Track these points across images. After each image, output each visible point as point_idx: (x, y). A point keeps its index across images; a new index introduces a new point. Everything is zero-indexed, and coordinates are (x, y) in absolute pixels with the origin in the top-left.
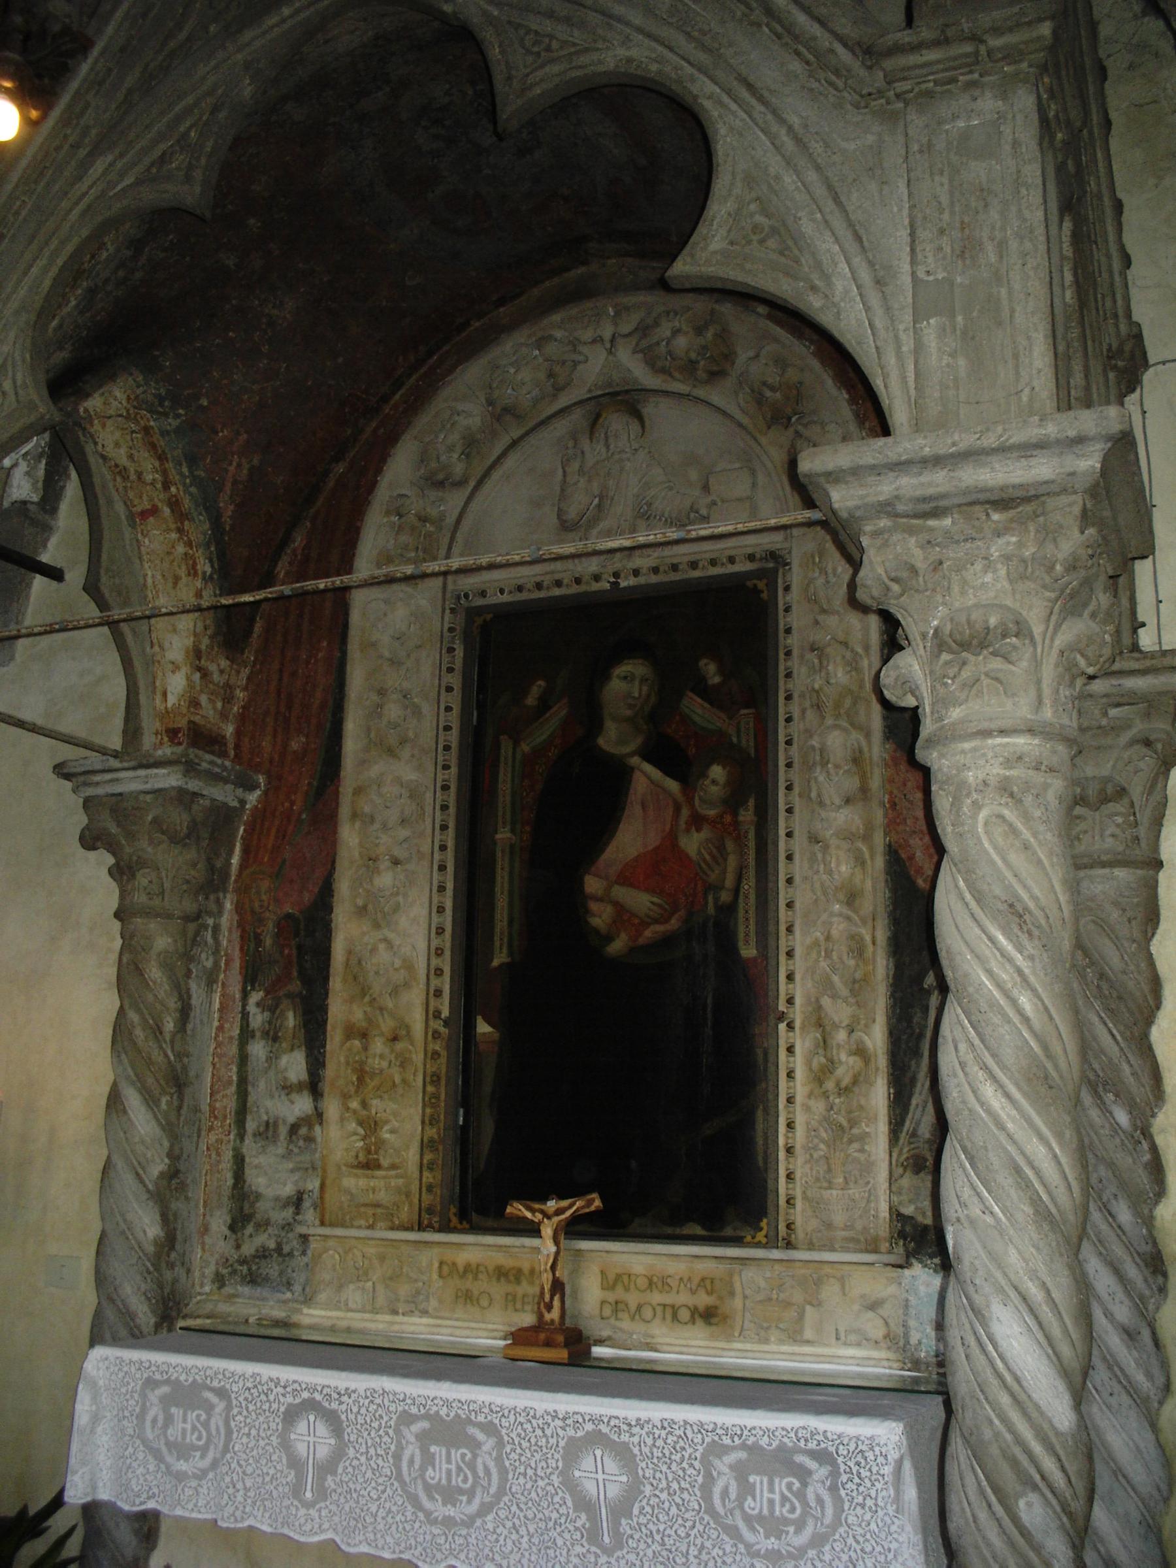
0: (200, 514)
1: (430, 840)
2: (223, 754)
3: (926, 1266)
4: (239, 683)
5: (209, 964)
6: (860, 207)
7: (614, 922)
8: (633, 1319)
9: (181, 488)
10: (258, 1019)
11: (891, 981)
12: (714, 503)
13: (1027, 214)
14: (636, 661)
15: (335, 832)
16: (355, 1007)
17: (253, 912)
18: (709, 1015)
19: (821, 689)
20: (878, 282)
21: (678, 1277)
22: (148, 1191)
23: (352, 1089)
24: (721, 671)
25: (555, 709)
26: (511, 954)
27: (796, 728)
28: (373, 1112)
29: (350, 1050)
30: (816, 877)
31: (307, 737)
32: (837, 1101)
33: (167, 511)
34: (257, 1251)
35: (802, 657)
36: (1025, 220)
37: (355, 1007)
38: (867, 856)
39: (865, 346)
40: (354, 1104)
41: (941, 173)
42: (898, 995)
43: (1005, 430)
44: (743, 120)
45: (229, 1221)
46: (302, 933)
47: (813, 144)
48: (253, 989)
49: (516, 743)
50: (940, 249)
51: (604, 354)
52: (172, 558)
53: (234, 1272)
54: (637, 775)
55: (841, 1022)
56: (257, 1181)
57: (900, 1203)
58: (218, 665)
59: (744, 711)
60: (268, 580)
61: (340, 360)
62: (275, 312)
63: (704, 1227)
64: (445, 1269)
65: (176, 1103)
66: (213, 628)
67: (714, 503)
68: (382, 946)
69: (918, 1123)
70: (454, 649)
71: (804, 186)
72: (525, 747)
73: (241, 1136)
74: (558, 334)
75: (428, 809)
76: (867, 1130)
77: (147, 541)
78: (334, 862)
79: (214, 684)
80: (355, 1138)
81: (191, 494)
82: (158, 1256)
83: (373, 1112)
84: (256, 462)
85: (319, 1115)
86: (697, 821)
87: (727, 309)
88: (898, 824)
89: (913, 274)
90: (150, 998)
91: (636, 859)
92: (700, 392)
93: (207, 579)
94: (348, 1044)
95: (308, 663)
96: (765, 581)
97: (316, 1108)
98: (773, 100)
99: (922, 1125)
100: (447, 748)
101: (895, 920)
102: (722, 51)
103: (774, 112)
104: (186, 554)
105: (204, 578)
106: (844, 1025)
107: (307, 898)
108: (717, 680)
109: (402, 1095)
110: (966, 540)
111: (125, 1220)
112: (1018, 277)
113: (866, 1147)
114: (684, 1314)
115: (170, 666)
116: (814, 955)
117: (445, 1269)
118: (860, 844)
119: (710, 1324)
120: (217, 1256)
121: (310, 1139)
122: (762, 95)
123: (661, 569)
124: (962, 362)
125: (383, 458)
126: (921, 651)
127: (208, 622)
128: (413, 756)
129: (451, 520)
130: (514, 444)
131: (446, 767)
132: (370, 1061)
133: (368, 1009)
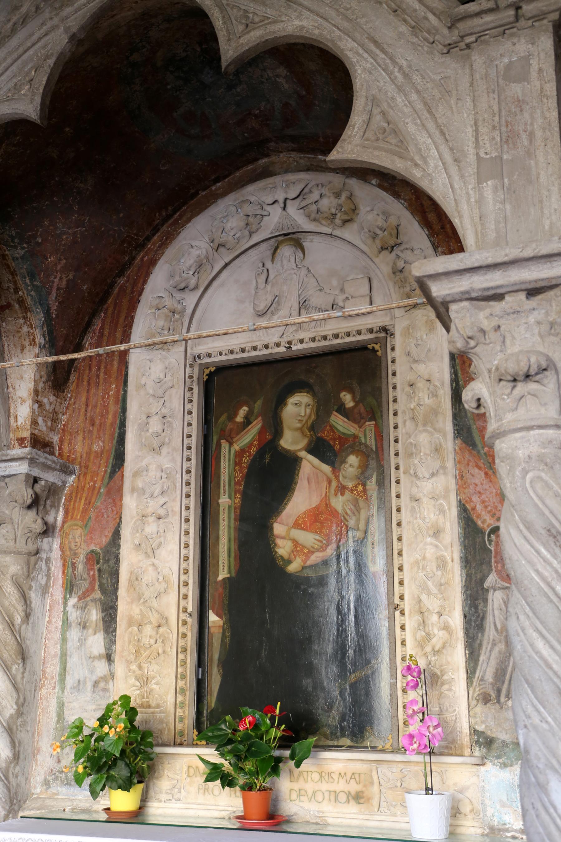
0: (37, 308)
1: (179, 503)
2: (52, 453)
3: (494, 764)
4: (61, 410)
5: (43, 582)
6: (444, 115)
7: (293, 551)
8: (310, 800)
9: (25, 292)
10: (74, 615)
11: (464, 584)
12: (347, 298)
13: (547, 114)
14: (302, 394)
15: (121, 500)
16: (134, 606)
17: (70, 549)
18: (352, 606)
19: (415, 408)
20: (456, 160)
21: (338, 773)
22: (4, 727)
23: (132, 657)
24: (354, 399)
25: (254, 423)
26: (229, 572)
27: (401, 431)
28: (146, 671)
29: (131, 633)
30: (415, 521)
31: (103, 442)
32: (433, 659)
33: (17, 306)
35: (403, 390)
36: (545, 118)
37: (134, 606)
38: (446, 508)
39: (448, 199)
40: (134, 667)
41: (494, 92)
42: (468, 592)
43: (537, 245)
44: (371, 64)
46: (101, 561)
47: (415, 77)
48: (70, 597)
49: (231, 444)
50: (494, 138)
52: (20, 335)
53: (56, 778)
55: (434, 610)
57: (476, 723)
58: (48, 399)
59: (368, 423)
60: (78, 348)
61: (121, 215)
63: (352, 740)
64: (192, 771)
65: (21, 670)
66: (45, 376)
67: (347, 298)
68: (151, 569)
69: (485, 673)
70: (192, 389)
71: (409, 102)
72: (236, 447)
73: (63, 689)
76: (453, 677)
77: (4, 324)
78: (121, 518)
79: (46, 411)
80: (134, 688)
83: (146, 671)
84: (71, 277)
85: (112, 676)
86: (342, 489)
87: (353, 183)
88: (465, 488)
89: (477, 154)
91: (305, 513)
92: (337, 233)
94: (130, 629)
96: (379, 345)
97: (110, 671)
98: (390, 50)
99: (487, 673)
100: (189, 448)
101: (465, 546)
102: (358, 20)
103: (391, 58)
104: (28, 332)
105: (40, 347)
106: (436, 611)
107: (105, 541)
109: (164, 661)
110: (514, 313)
112: (542, 154)
113: (453, 688)
116: (415, 569)
117: (192, 771)
118: (441, 501)
119: (359, 803)
120: (46, 769)
121: (105, 690)
122: (383, 48)
123: (317, 339)
124: (508, 207)
125: (147, 275)
126: (487, 380)
127: (43, 373)
128: (168, 453)
129: (189, 311)
130: (226, 265)
131: (189, 459)
133: (142, 608)
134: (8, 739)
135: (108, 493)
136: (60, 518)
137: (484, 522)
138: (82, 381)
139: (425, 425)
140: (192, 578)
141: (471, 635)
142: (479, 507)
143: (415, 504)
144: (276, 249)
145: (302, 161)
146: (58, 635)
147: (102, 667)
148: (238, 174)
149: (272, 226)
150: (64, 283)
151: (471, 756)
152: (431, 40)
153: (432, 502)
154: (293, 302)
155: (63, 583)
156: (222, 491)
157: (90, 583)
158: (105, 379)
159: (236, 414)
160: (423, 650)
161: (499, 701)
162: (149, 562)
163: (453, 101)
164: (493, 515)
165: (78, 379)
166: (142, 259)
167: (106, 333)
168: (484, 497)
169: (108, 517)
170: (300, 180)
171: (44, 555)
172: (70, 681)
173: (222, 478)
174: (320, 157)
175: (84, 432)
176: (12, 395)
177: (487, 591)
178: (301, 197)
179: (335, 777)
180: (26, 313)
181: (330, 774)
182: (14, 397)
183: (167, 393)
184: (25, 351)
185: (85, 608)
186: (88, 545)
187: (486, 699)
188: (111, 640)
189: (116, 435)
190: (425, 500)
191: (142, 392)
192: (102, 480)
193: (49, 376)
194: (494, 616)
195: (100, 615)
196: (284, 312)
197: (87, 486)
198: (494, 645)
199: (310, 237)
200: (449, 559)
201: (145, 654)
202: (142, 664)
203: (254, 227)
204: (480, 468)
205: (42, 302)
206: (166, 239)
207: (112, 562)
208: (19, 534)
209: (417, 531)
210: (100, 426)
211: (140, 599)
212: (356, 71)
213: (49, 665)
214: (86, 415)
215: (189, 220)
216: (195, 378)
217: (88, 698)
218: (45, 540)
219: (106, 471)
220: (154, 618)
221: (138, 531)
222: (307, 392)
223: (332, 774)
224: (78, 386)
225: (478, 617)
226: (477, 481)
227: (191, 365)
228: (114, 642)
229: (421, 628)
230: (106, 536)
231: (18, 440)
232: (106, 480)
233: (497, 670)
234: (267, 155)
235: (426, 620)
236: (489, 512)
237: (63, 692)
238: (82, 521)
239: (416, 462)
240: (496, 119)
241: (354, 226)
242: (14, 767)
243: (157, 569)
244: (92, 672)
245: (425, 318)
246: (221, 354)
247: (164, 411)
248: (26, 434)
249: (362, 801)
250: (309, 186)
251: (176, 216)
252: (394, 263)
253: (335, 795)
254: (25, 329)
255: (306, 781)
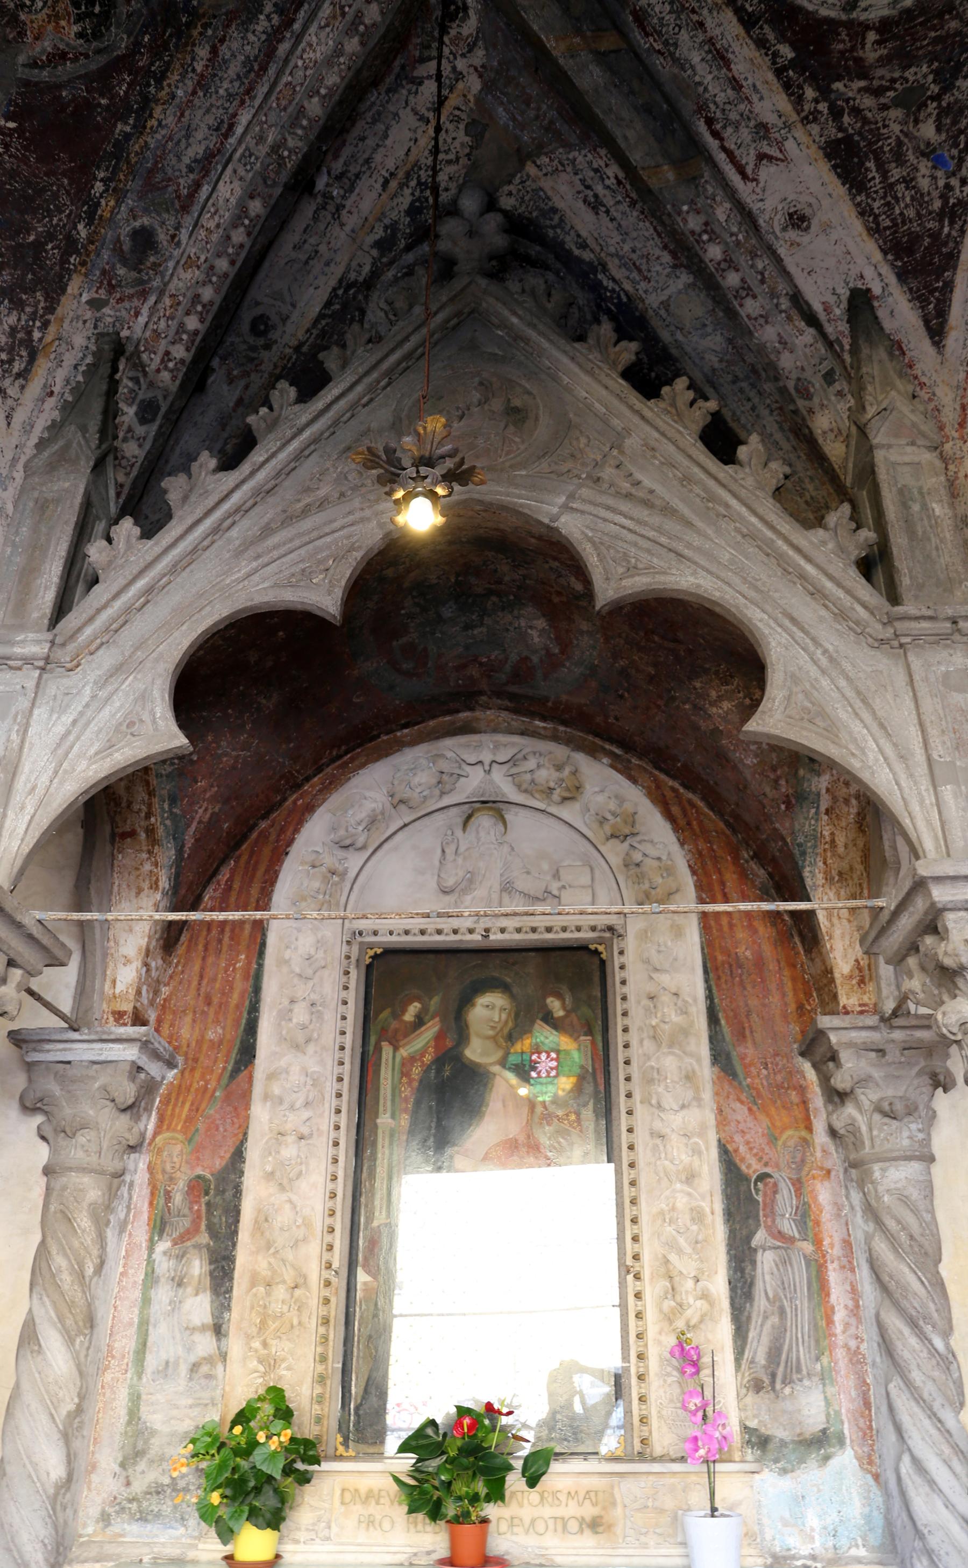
5: (122, 1216)
8: (527, 1532)
10: (164, 1265)
12: (564, 887)
15: (247, 1107)
16: (260, 1258)
17: (164, 1171)
19: (657, 1025)
21: (566, 1491)
23: (254, 1330)
24: (564, 1007)
28: (274, 1351)
29: (255, 1295)
31: (224, 1028)
34: (149, 1487)
35: (639, 1002)
37: (260, 1258)
38: (703, 1148)
40: (256, 1344)
42: (732, 1252)
45: (120, 1459)
46: (212, 1192)
48: (160, 1238)
49: (396, 1049)
50: (944, 743)
51: (482, 773)
54: (498, 1079)
56: (154, 1418)
62: (264, 701)
65: (86, 1344)
67: (564, 887)
68: (287, 1206)
69: (755, 1353)
73: (140, 1374)
74: (450, 754)
75: (327, 1096)
78: (245, 1134)
80: (256, 1375)
81: (165, 826)
82: (56, 1495)
83: (274, 1351)
84: (217, 810)
85: (224, 1357)
90: (76, 1244)
93: (165, 894)
94: (254, 1290)
95: (226, 970)
103: (813, 639)
107: (219, 1164)
108: (561, 1013)
111: (31, 1462)
114: (573, 1526)
115: (123, 960)
116: (659, 1222)
117: (348, 1496)
119: (597, 1533)
129: (352, 874)
130: (405, 825)
132: (273, 1305)
133: (272, 1260)
134: (64, 1450)
135: (227, 1098)
136: (151, 1127)
137: (749, 1166)
138: (196, 944)
139: (671, 1046)
140: (341, 1223)
141: (737, 1306)
142: (743, 1149)
143: (658, 1141)
144: (469, 817)
145: (513, 723)
146: (136, 1294)
147: (205, 1344)
148: (432, 723)
149: (469, 790)
150: (208, 816)
151: (742, 1461)
152: (859, 631)
153: (684, 1140)
154: (494, 881)
155: (149, 1219)
156: (381, 1108)
157: (193, 1221)
158: (231, 946)
159: (404, 1011)
160: (671, 1324)
161: (773, 1389)
162: (284, 1197)
163: (889, 696)
164: (760, 1159)
165: (190, 941)
166: (295, 802)
167: (236, 886)
168: (748, 1137)
169: (225, 1130)
170: (513, 744)
171: (127, 1178)
172: (152, 1362)
173: (382, 1092)
174: (537, 722)
175: (195, 1012)
176: (113, 951)
177: (755, 1250)
178: (511, 763)
179: (563, 1497)
180: (153, 846)
181: (555, 1494)
182: (116, 955)
183: (318, 974)
184: (142, 895)
185: (183, 1256)
186: (192, 1168)
187: (757, 1386)
188: (222, 1304)
189: (244, 1021)
190: (674, 1137)
191: (285, 969)
192: (219, 1080)
193: (163, 932)
194: (764, 1282)
195: (207, 1268)
196: (480, 892)
197: (195, 1085)
198: (766, 1318)
199: (514, 809)
200: (708, 1210)
201: (273, 1326)
202: (268, 1341)
203: (448, 787)
204: (742, 1102)
205: (177, 836)
206: (330, 783)
207: (229, 1194)
208: (105, 1145)
209: (662, 1175)
210: (220, 1007)
211: (269, 1248)
212: (769, 643)
213: (118, 1337)
214: (198, 989)
215: (363, 766)
216: (353, 959)
217: (181, 1389)
218: (132, 1156)
219: (224, 1068)
220: (289, 1276)
221: (270, 1154)
222: (503, 992)
223: (559, 1495)
224: (188, 950)
225: (745, 1283)
226: (739, 1118)
227: (348, 943)
228: (229, 1308)
229: (669, 1296)
230: (221, 1157)
231: (114, 1013)
232: (224, 1081)
233: (770, 1349)
234: (472, 709)
235: (676, 1285)
236: (755, 1155)
237: (140, 1378)
238: (185, 1133)
239: (660, 1090)
240: (943, 723)
241: (577, 806)
242: (64, 1494)
243: (295, 1207)
244: (189, 1350)
245: (669, 922)
246: (391, 933)
247: (314, 997)
248: (127, 1007)
249: (601, 1529)
250: (523, 752)
251: (346, 758)
252: (627, 854)
253: (562, 1524)
254: (147, 867)
255: (521, 1505)
